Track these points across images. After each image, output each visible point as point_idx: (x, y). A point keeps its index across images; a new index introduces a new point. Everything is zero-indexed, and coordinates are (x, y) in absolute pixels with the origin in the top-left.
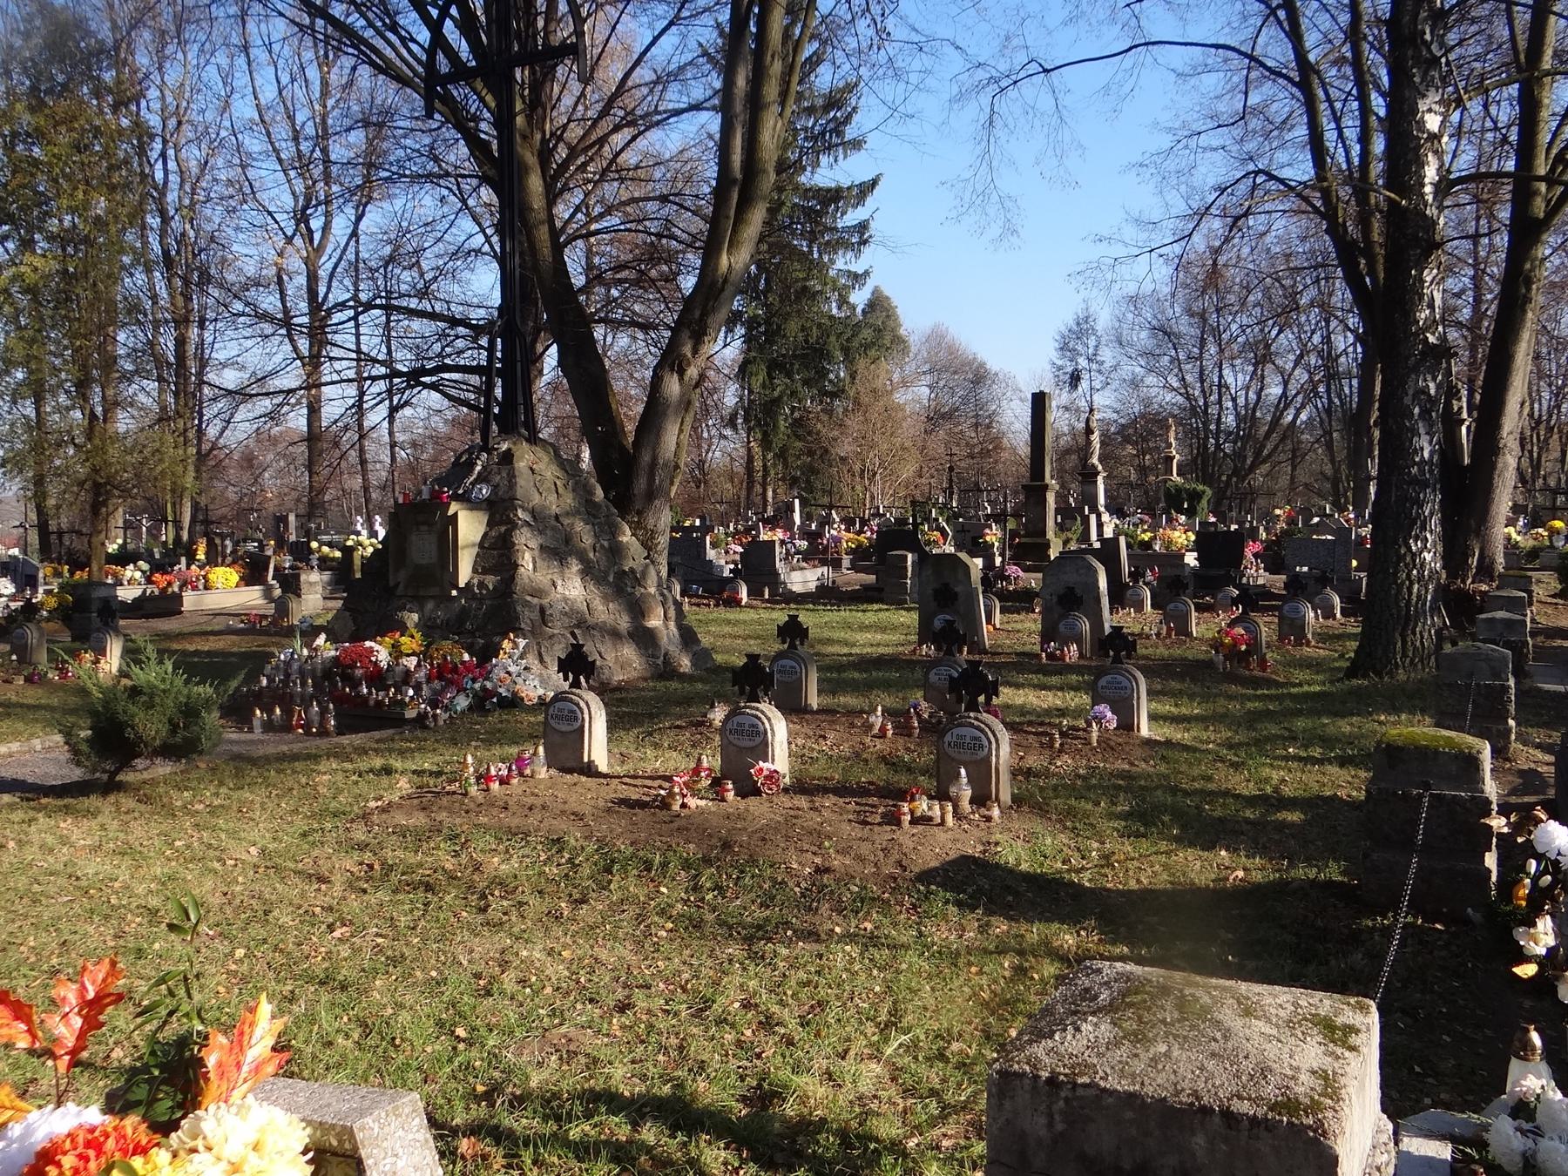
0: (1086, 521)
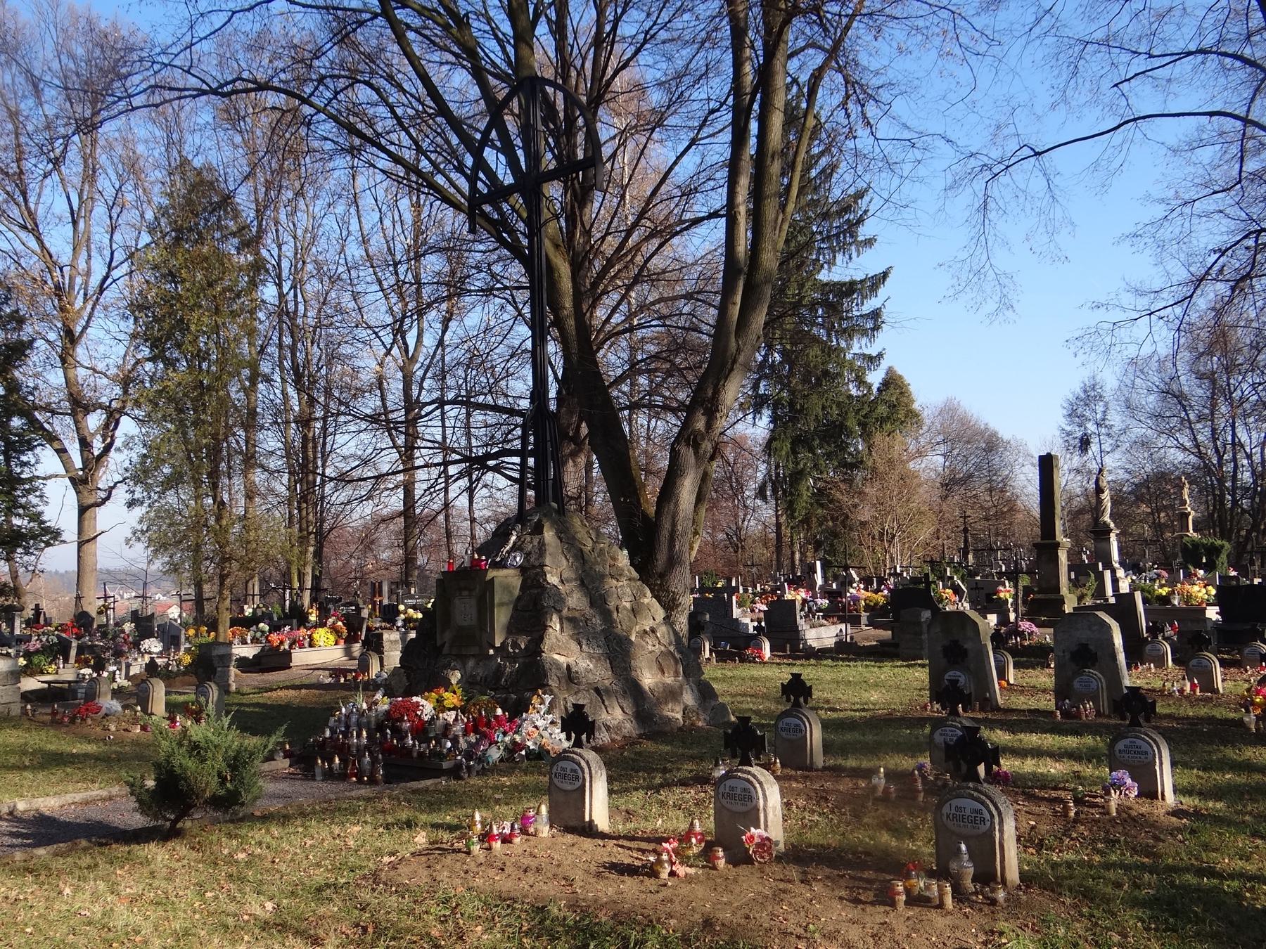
0: (1100, 578)
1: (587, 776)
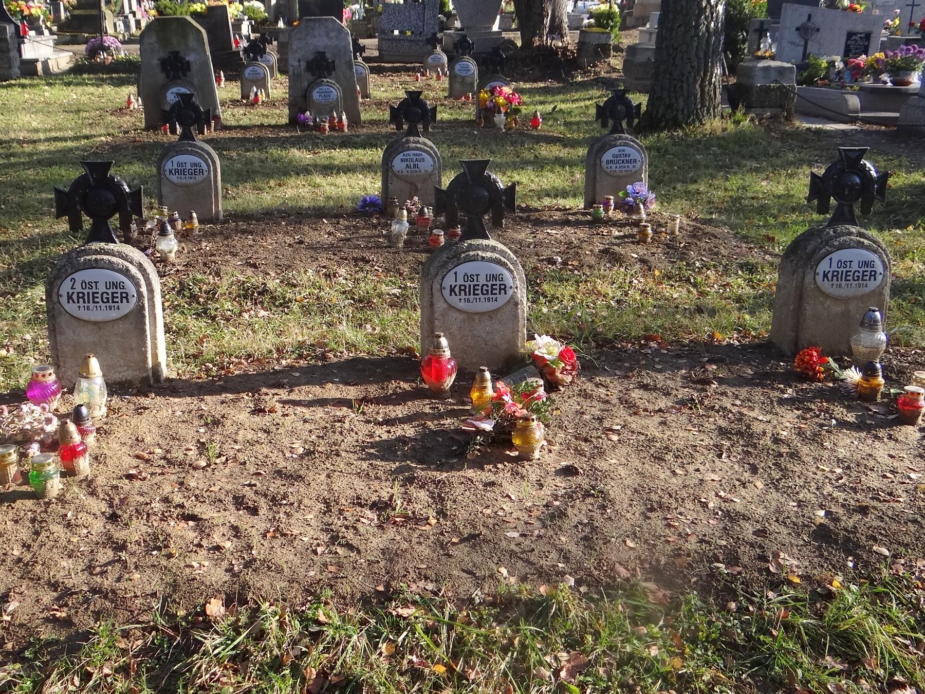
1: (144, 289)
